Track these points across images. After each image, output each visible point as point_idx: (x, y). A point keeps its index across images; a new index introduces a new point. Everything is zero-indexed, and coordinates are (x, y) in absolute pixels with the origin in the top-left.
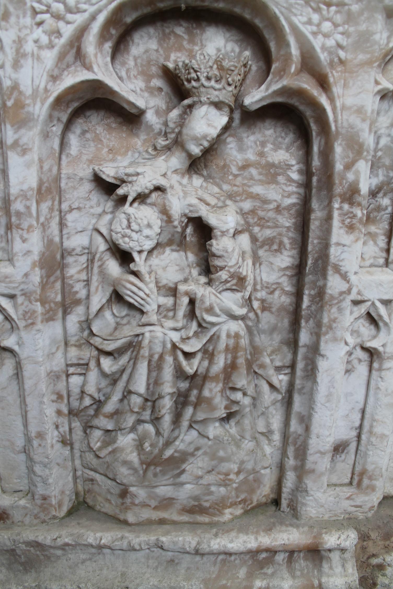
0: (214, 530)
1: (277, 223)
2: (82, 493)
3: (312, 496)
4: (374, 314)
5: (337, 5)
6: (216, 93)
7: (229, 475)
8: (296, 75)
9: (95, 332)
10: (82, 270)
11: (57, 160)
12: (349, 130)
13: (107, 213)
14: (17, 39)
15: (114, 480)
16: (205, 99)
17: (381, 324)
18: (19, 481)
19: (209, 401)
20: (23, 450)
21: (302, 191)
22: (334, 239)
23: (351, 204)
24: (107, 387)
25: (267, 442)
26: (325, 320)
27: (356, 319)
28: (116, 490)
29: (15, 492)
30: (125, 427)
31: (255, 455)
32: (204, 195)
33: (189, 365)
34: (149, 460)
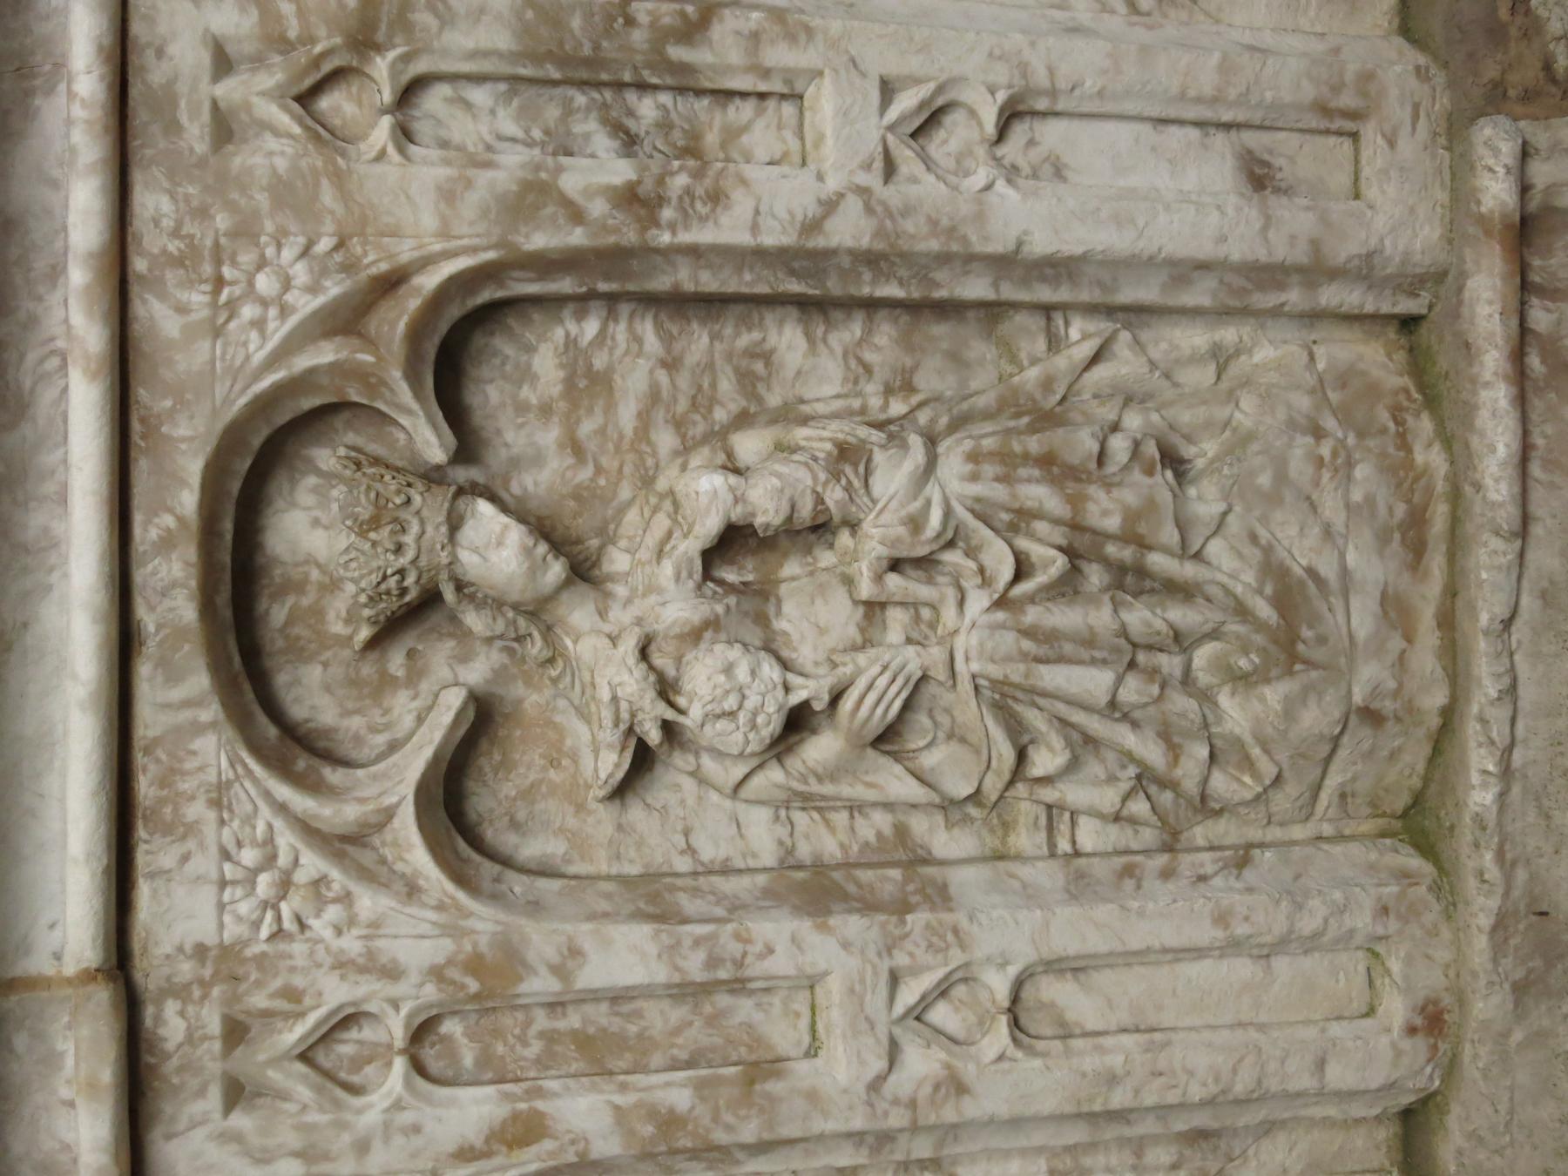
0: (1468, 489)
1: (702, 365)
2: (1380, 821)
3: (1382, 240)
4: (917, 123)
5: (218, 262)
6: (429, 529)
7: (1321, 459)
8: (377, 349)
9: (971, 790)
10: (827, 822)
11: (587, 882)
12: (492, 216)
13: (699, 766)
14: (337, 972)
15: (1336, 742)
16: (444, 554)
17: (940, 102)
18: (1342, 973)
19: (1132, 517)
20: (1263, 962)
21: (625, 309)
22: (744, 238)
23: (661, 200)
24: (1103, 761)
25: (1243, 358)
26: (934, 245)
27: (928, 169)
28: (1360, 737)
29: (1371, 983)
30: (1200, 715)
31: (1274, 391)
32: (650, 544)
33: (1046, 566)
34: (1283, 657)
